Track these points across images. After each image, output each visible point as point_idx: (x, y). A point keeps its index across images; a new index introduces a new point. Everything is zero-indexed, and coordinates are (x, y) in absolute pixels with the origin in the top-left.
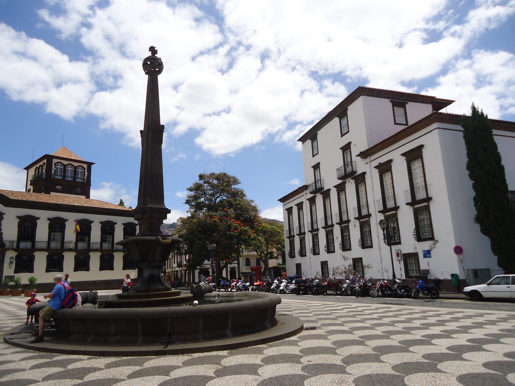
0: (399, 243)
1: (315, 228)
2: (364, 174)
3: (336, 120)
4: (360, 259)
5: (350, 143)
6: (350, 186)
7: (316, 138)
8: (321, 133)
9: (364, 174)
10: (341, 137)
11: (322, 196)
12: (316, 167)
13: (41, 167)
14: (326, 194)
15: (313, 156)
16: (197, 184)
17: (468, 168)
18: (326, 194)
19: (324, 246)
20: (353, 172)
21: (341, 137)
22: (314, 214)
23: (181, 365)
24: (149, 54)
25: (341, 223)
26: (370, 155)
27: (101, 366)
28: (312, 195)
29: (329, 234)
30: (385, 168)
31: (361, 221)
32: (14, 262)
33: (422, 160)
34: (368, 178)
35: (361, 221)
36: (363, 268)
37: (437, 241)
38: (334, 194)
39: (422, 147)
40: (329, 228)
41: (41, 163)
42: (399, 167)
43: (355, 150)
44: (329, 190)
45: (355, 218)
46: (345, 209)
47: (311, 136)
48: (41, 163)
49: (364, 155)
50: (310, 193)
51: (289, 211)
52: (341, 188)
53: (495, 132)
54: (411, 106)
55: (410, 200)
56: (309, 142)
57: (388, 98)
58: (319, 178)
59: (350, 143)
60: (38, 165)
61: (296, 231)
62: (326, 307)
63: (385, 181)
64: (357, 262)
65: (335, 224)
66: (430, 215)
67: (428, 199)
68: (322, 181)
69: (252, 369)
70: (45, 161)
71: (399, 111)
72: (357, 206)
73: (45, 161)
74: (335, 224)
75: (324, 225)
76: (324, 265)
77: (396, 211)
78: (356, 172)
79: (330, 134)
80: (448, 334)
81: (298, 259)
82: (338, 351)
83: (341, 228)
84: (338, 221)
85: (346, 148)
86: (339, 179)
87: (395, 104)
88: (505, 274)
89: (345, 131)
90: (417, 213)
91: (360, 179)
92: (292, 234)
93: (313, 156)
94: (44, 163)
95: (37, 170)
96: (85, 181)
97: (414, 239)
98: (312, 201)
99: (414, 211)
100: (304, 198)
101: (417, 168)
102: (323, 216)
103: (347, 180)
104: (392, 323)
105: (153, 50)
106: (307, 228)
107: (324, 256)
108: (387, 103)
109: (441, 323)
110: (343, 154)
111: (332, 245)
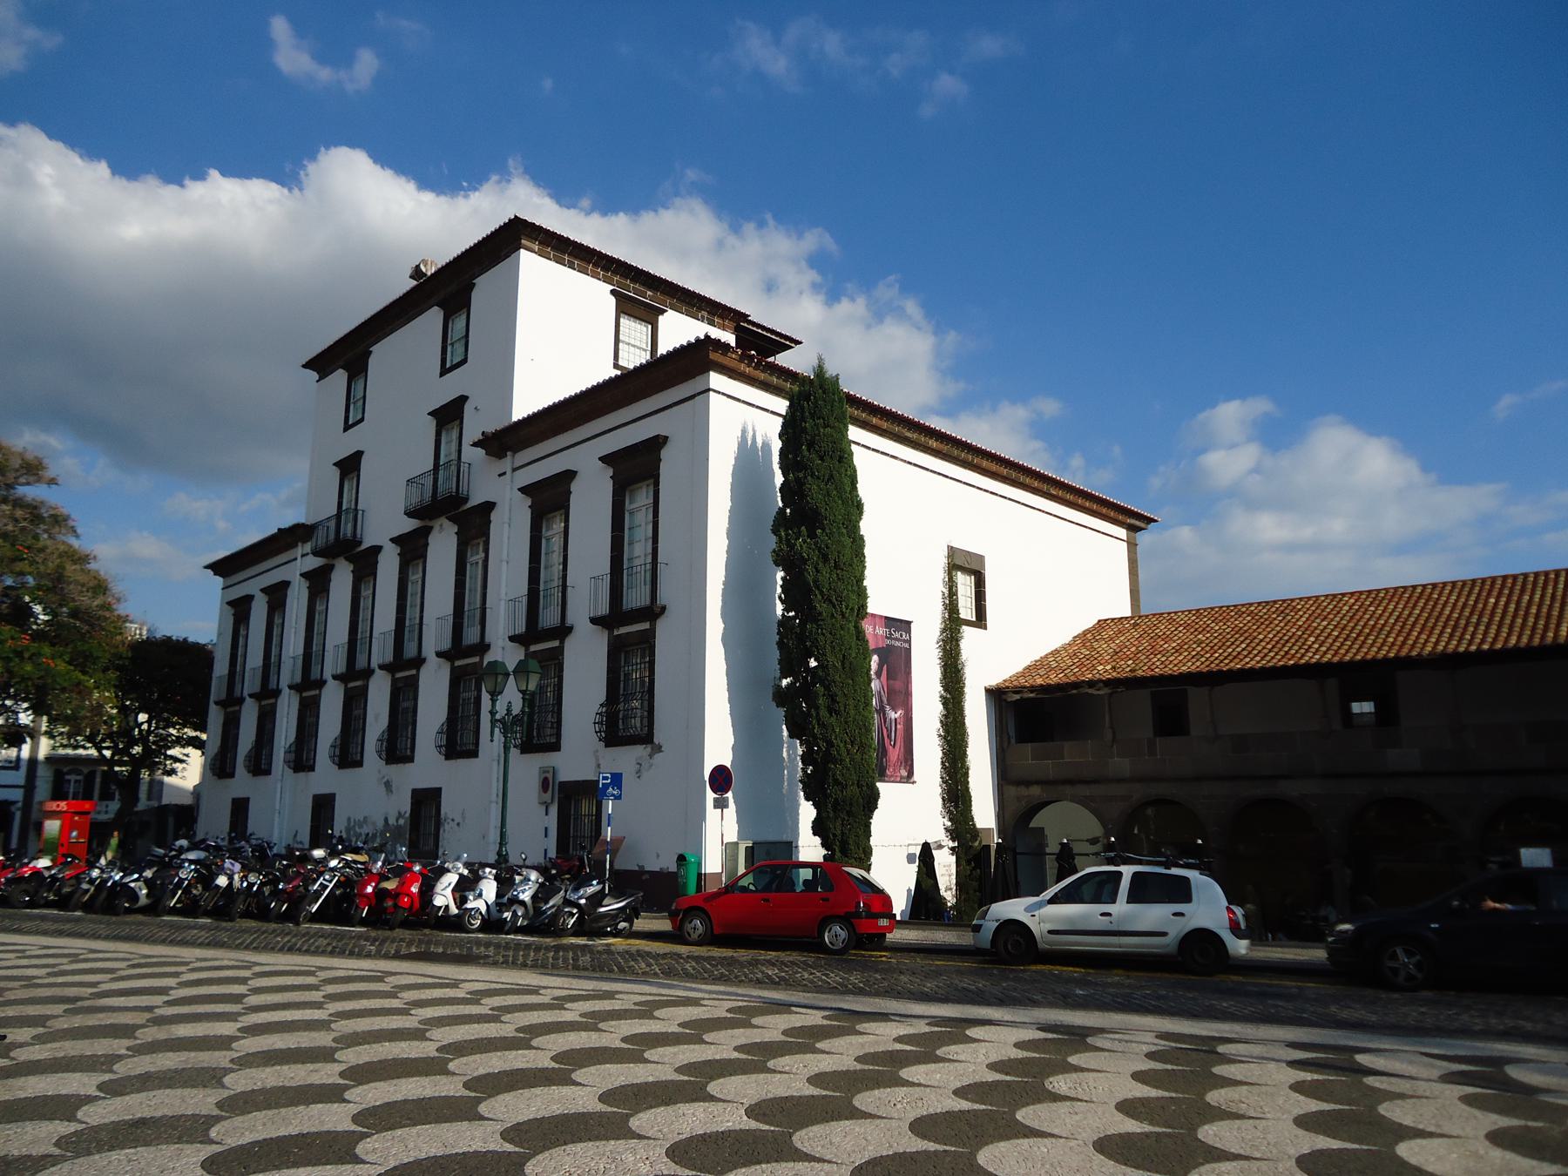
0: (555, 747)
2: (489, 506)
4: (435, 794)
5: (463, 399)
6: (443, 544)
7: (467, 305)
8: (383, 355)
9: (489, 506)
10: (345, 430)
12: (350, 466)
14: (366, 563)
15: (347, 427)
17: (859, 507)
19: (437, 727)
20: (458, 499)
21: (345, 430)
26: (517, 448)
29: (355, 703)
30: (550, 499)
31: (457, 663)
33: (657, 484)
35: (457, 663)
36: (438, 824)
37: (659, 749)
39: (658, 442)
40: (355, 677)
42: (592, 499)
43: (475, 425)
44: (377, 550)
45: (594, 621)
46: (556, 582)
47: (348, 356)
49: (509, 440)
50: (316, 553)
51: (240, 609)
52: (412, 548)
55: (521, 628)
56: (340, 377)
58: (454, 456)
59: (463, 399)
61: (334, 662)
63: (631, 513)
64: (426, 801)
65: (286, 691)
66: (652, 663)
67: (653, 612)
68: (464, 468)
71: (635, 331)
74: (286, 691)
75: (341, 668)
76: (323, 806)
77: (562, 642)
78: (466, 500)
79: (407, 365)
81: (326, 776)
83: (394, 682)
85: (449, 415)
86: (410, 514)
87: (626, 306)
89: (454, 357)
90: (618, 652)
91: (474, 524)
98: (318, 582)
100: (304, 560)
101: (639, 509)
102: (390, 625)
103: (436, 524)
106: (289, 672)
108: (598, 294)
111: (471, 726)
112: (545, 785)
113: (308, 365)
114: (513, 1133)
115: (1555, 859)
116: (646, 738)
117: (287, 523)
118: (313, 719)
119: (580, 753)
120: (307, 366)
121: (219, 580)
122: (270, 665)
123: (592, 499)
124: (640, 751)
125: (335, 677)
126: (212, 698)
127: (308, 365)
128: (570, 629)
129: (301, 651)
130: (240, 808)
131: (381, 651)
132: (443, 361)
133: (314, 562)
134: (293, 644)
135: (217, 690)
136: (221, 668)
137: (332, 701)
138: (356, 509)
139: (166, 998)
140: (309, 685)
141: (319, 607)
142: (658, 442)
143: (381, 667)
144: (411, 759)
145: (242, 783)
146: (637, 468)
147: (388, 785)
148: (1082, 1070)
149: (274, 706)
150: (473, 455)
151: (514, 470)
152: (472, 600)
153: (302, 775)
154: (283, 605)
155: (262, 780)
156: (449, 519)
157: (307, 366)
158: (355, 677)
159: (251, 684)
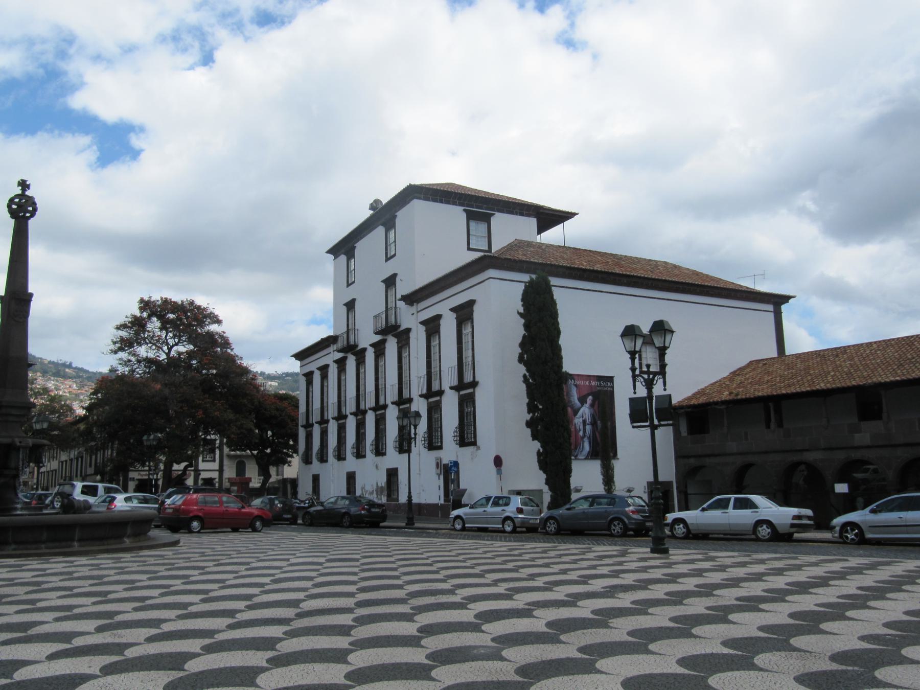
0: (440, 448)
1: (435, 387)
3: (380, 230)
6: (392, 345)
8: (361, 247)
11: (396, 340)
12: (350, 306)
14: (360, 355)
15: (387, 259)
16: (135, 317)
18: (360, 355)
20: (397, 326)
22: (435, 357)
23: (98, 673)
24: (18, 191)
25: (460, 386)
26: (419, 301)
28: (340, 355)
30: (432, 326)
33: (472, 322)
34: (412, 335)
39: (471, 303)
40: (360, 413)
42: (448, 326)
44: (364, 350)
45: (421, 396)
46: (470, 359)
47: (345, 248)
49: (412, 299)
51: (309, 376)
52: (380, 349)
53: (554, 281)
54: (499, 220)
55: (424, 391)
57: (461, 205)
61: (350, 407)
62: (470, 559)
67: (474, 384)
71: (478, 228)
76: (392, 474)
78: (399, 326)
80: (721, 615)
81: (351, 464)
84: (396, 399)
85: (390, 282)
86: (376, 333)
87: (471, 216)
88: (899, 492)
91: (403, 337)
92: (382, 402)
93: (387, 259)
97: (454, 444)
98: (341, 363)
100: (330, 357)
102: (319, 406)
104: (610, 592)
105: (24, 185)
107: (393, 458)
108: (456, 214)
109: (707, 590)
112: (437, 464)
113: (329, 252)
114: (522, 671)
115: (849, 488)
116: (474, 444)
117: (324, 336)
120: (328, 252)
121: (298, 362)
123: (448, 326)
124: (471, 448)
126: (300, 424)
127: (329, 252)
129: (425, 372)
130: (316, 479)
131: (370, 402)
132: (386, 253)
134: (333, 398)
135: (302, 420)
136: (302, 408)
137: (333, 427)
138: (396, 307)
141: (362, 371)
143: (370, 409)
146: (464, 313)
147: (377, 467)
148: (767, 611)
149: (327, 428)
150: (401, 304)
152: (405, 378)
154: (364, 362)
155: (309, 466)
156: (393, 336)
157: (328, 252)
158: (360, 413)
159: (316, 417)
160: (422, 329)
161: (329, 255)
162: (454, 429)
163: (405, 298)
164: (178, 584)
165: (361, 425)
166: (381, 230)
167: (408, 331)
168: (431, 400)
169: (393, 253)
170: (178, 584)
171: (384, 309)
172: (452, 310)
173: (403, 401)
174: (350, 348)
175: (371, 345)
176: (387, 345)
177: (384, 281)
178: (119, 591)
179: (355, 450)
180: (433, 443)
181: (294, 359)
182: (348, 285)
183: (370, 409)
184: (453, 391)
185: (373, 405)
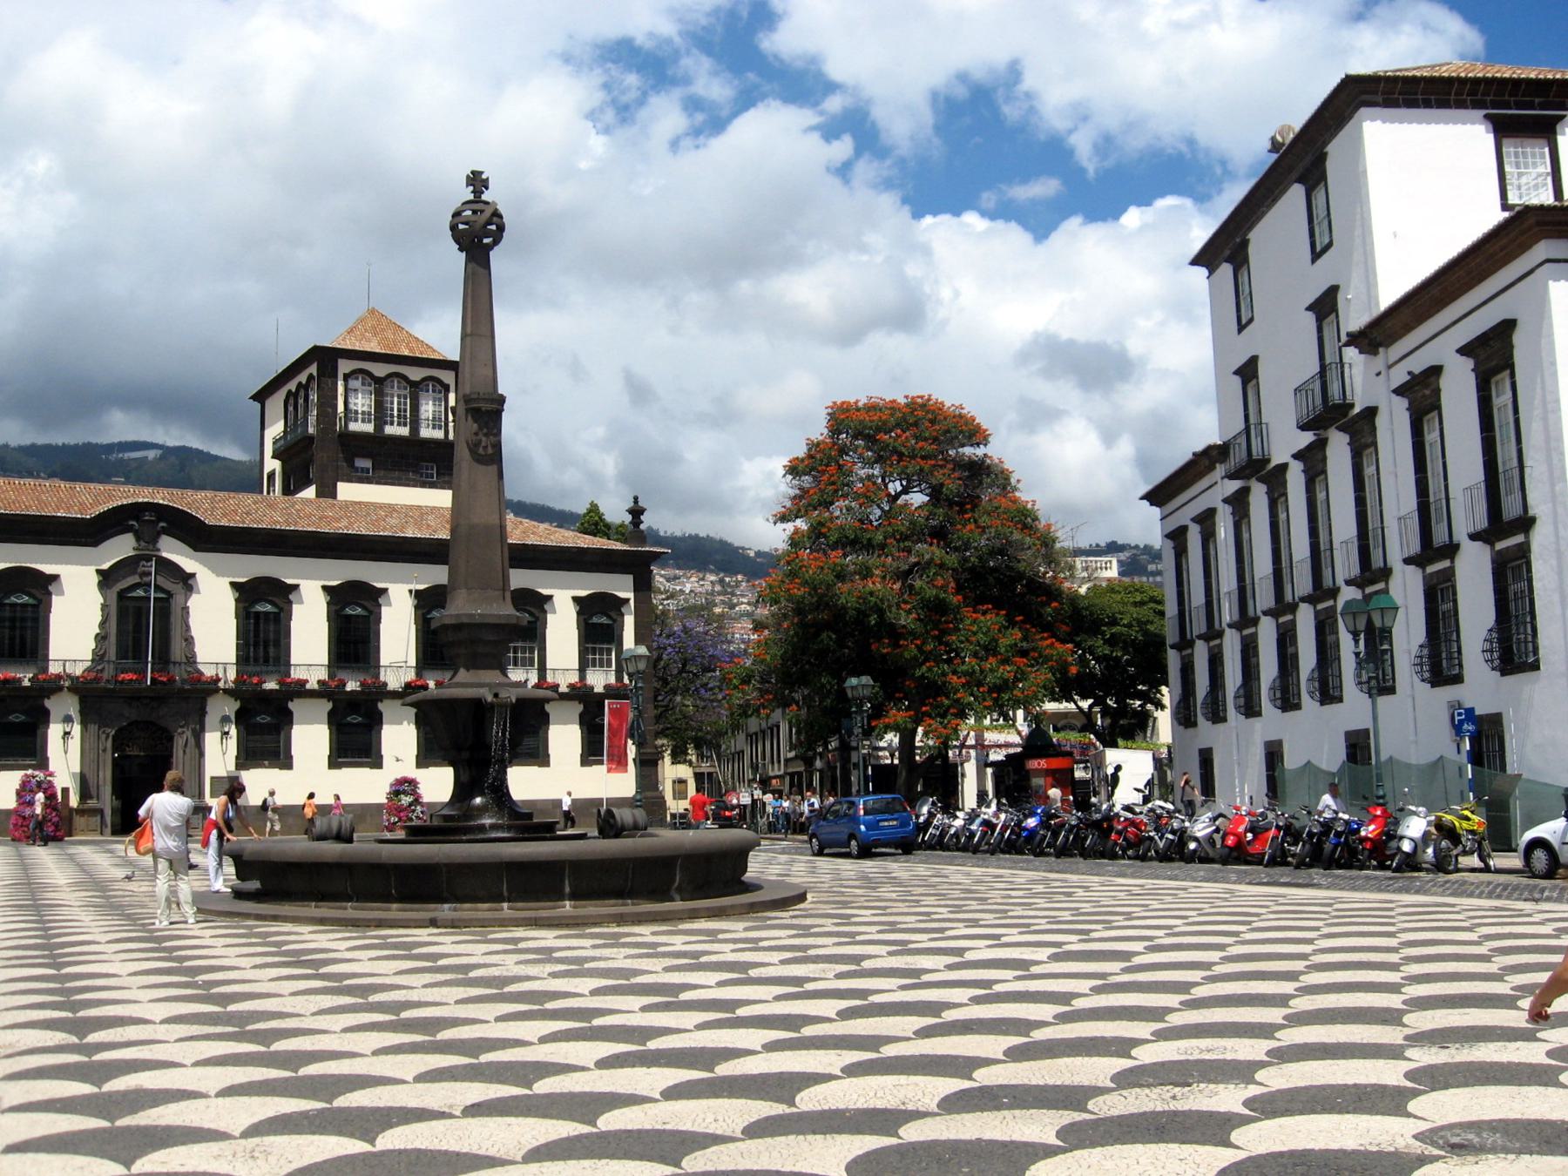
0: (1458, 679)
6: (1339, 448)
10: (1313, 261)
12: (1248, 372)
13: (302, 393)
14: (1275, 479)
21: (1313, 261)
27: (286, 992)
28: (1234, 485)
29: (1439, 596)
30: (1422, 394)
32: (233, 731)
33: (1513, 375)
34: (1381, 421)
38: (1295, 479)
39: (1508, 326)
40: (1433, 552)
41: (303, 378)
44: (1283, 468)
48: (303, 378)
49: (1377, 335)
50: (1231, 476)
51: (1177, 537)
52: (1312, 459)
56: (1226, 270)
57: (1477, 105)
60: (292, 386)
61: (1264, 597)
67: (1526, 523)
69: (1215, 1128)
70: (313, 369)
72: (1308, 554)
73: (313, 369)
77: (1527, 537)
78: (1268, 461)
81: (1271, 723)
82: (1409, 1053)
85: (1325, 306)
86: (1303, 427)
87: (1503, 129)
93: (1316, 255)
94: (311, 377)
95: (291, 401)
96: (451, 436)
97: (1486, 668)
99: (1493, 562)
100: (1218, 489)
106: (1399, 541)
110: (1320, 330)
113: (1196, 261)
118: (1524, 585)
119: (1481, 687)
121: (1156, 512)
122: (1244, 593)
125: (1474, 537)
127: (1196, 261)
128: (1532, 520)
129: (1270, 570)
130: (1206, 758)
133: (1233, 486)
137: (1231, 645)
139: (1209, 973)
140: (1433, 552)
142: (1508, 326)
143: (1230, 626)
144: (1535, 666)
145: (1206, 733)
146: (1494, 354)
150: (1351, 353)
151: (1390, 367)
153: (1251, 720)
154: (1436, 406)
156: (1340, 429)
160: (1401, 404)
161: (1196, 268)
162: (1484, 634)
163: (1355, 339)
164: (1008, 981)
165: (1286, 639)
166: (1296, 193)
167: (1371, 412)
168: (1431, 569)
169: (1327, 241)
170: (1008, 981)
171: (1242, 426)
172: (1464, 351)
173: (1322, 592)
174: (1257, 468)
175: (1193, 520)
176: (1329, 452)
177: (1236, 373)
178: (872, 933)
179: (1242, 701)
180: (1441, 667)
181: (1145, 503)
182: (1241, 328)
183: (1265, 613)
184: (1478, 544)
185: (1203, 629)
